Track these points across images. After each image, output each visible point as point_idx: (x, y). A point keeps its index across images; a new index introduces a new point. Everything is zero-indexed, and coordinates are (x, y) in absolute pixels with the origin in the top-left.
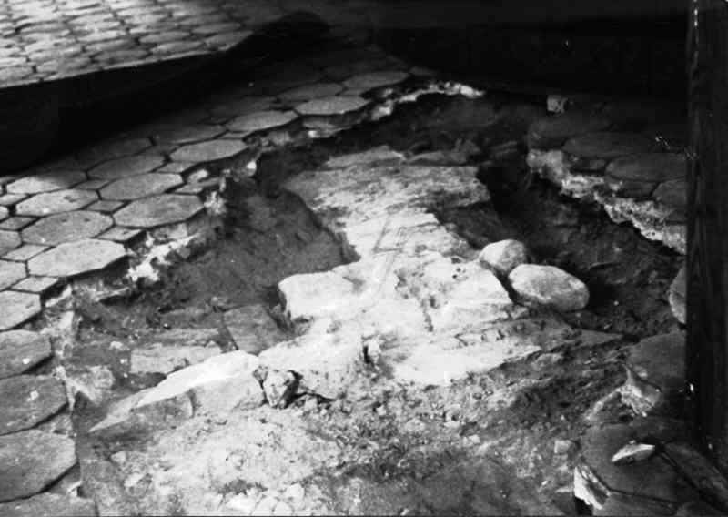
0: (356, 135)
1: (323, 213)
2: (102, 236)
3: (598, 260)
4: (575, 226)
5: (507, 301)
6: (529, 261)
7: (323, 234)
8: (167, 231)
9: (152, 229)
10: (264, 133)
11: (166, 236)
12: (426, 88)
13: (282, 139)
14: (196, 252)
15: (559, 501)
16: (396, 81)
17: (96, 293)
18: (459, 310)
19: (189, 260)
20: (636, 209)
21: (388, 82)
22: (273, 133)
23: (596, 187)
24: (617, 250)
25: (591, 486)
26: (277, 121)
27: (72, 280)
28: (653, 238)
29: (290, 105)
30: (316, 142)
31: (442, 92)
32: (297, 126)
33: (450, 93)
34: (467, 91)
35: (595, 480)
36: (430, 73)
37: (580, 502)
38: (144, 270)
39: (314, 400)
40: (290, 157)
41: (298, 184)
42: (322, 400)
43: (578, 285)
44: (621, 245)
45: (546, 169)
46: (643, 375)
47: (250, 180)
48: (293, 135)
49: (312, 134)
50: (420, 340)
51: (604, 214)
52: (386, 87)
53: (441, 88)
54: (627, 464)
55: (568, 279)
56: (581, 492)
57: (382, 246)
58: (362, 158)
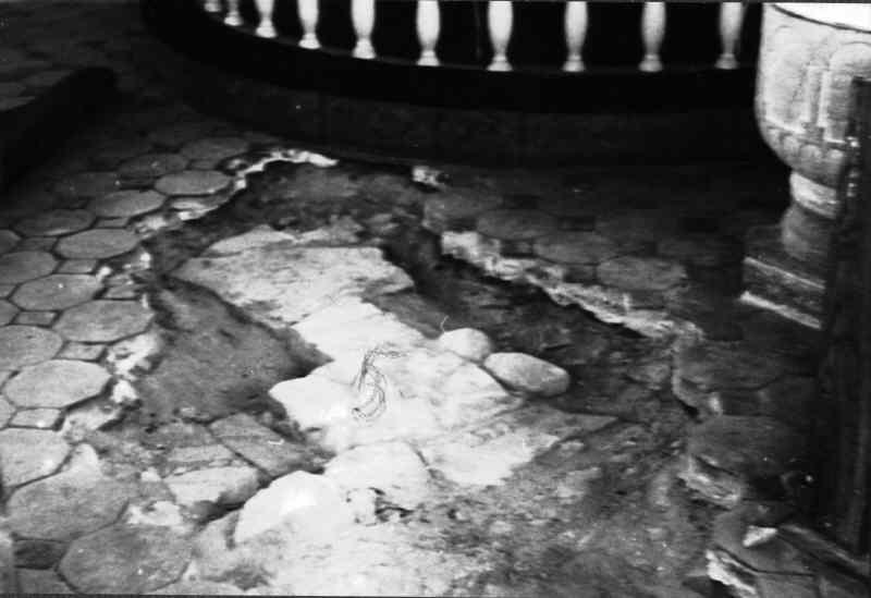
0: (232, 216)
1: (248, 307)
2: (62, 355)
3: (545, 341)
4: (506, 308)
5: (502, 393)
6: (496, 351)
7: (256, 331)
8: (126, 344)
9: (112, 343)
10: (139, 218)
11: (125, 349)
12: (269, 156)
13: (157, 223)
14: (155, 361)
15: (692, 584)
16: (242, 150)
17: (94, 419)
18: (464, 407)
19: (150, 372)
20: (585, 292)
21: (236, 153)
22: (149, 218)
23: (530, 271)
24: (565, 331)
25: (732, 569)
26: (146, 205)
27: (71, 408)
28: (609, 321)
29: (147, 182)
30: (189, 223)
31: (286, 159)
32: (167, 211)
33: (295, 161)
34: (319, 160)
35: (737, 565)
36: (270, 140)
37: (718, 584)
38: (124, 392)
39: (397, 514)
40: (169, 241)
41: (195, 271)
42: (404, 513)
43: (559, 372)
44: (568, 325)
45: (461, 250)
46: (713, 462)
47: (149, 273)
48: (167, 217)
49: (184, 216)
50: (442, 440)
51: (546, 297)
52: (232, 158)
53: (286, 155)
54: (758, 547)
55: (544, 366)
56: (717, 572)
57: (488, 364)
58: (246, 240)
